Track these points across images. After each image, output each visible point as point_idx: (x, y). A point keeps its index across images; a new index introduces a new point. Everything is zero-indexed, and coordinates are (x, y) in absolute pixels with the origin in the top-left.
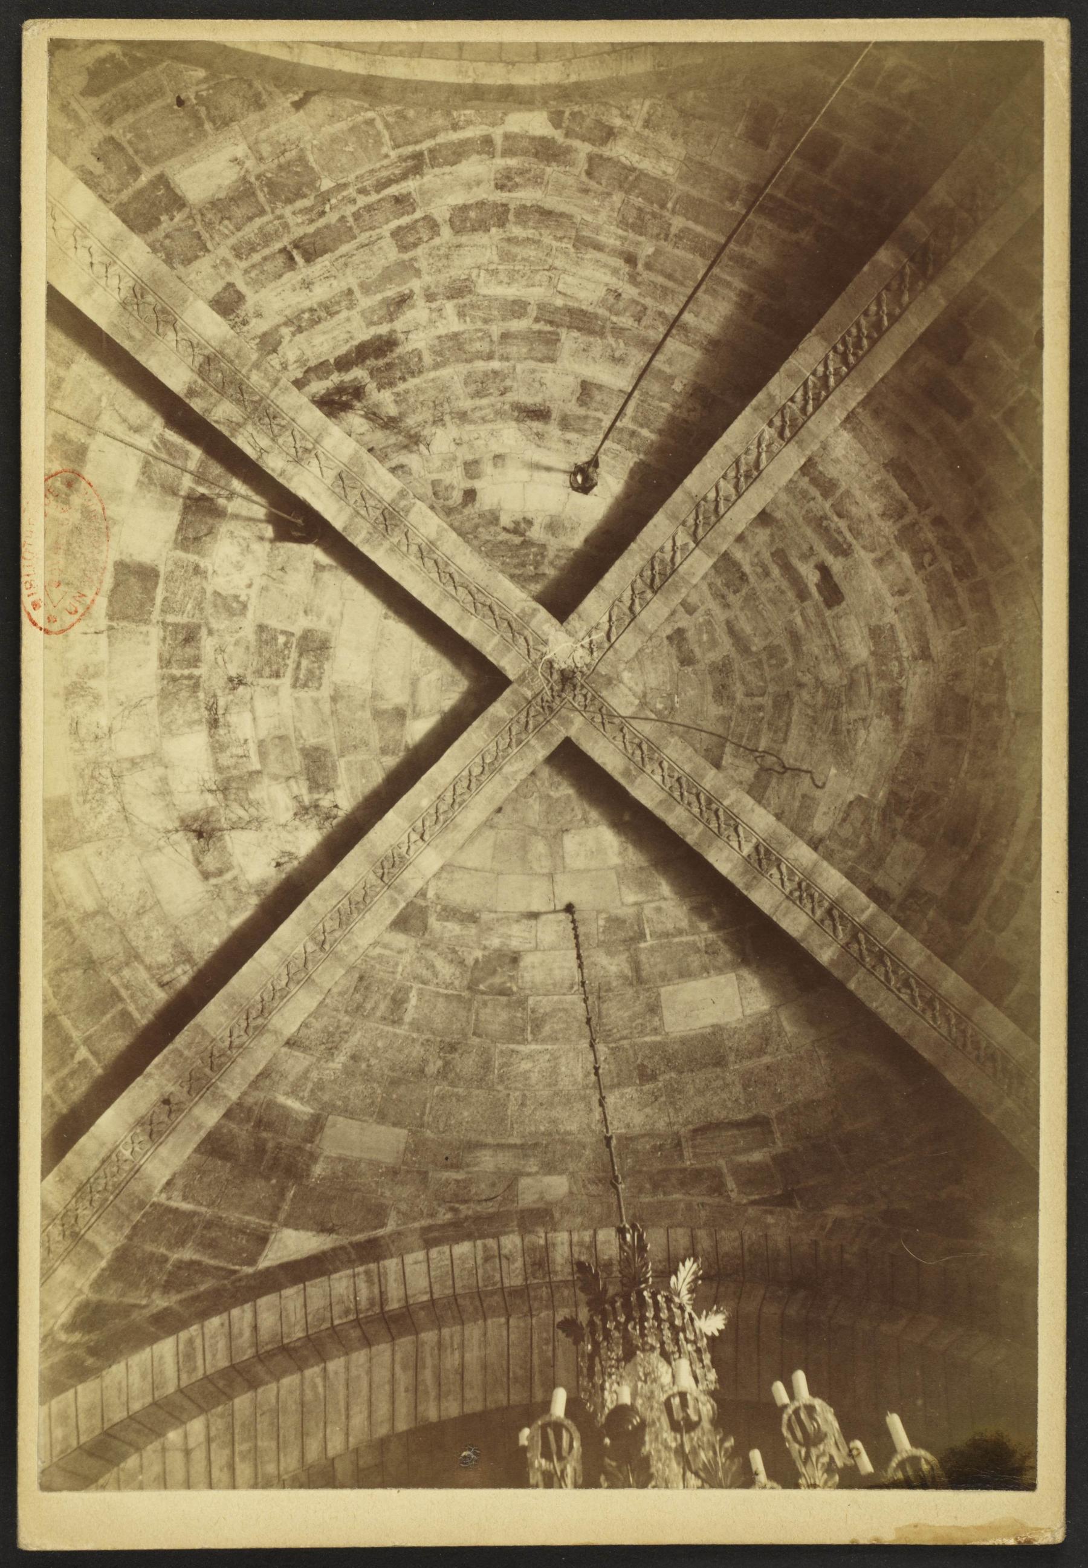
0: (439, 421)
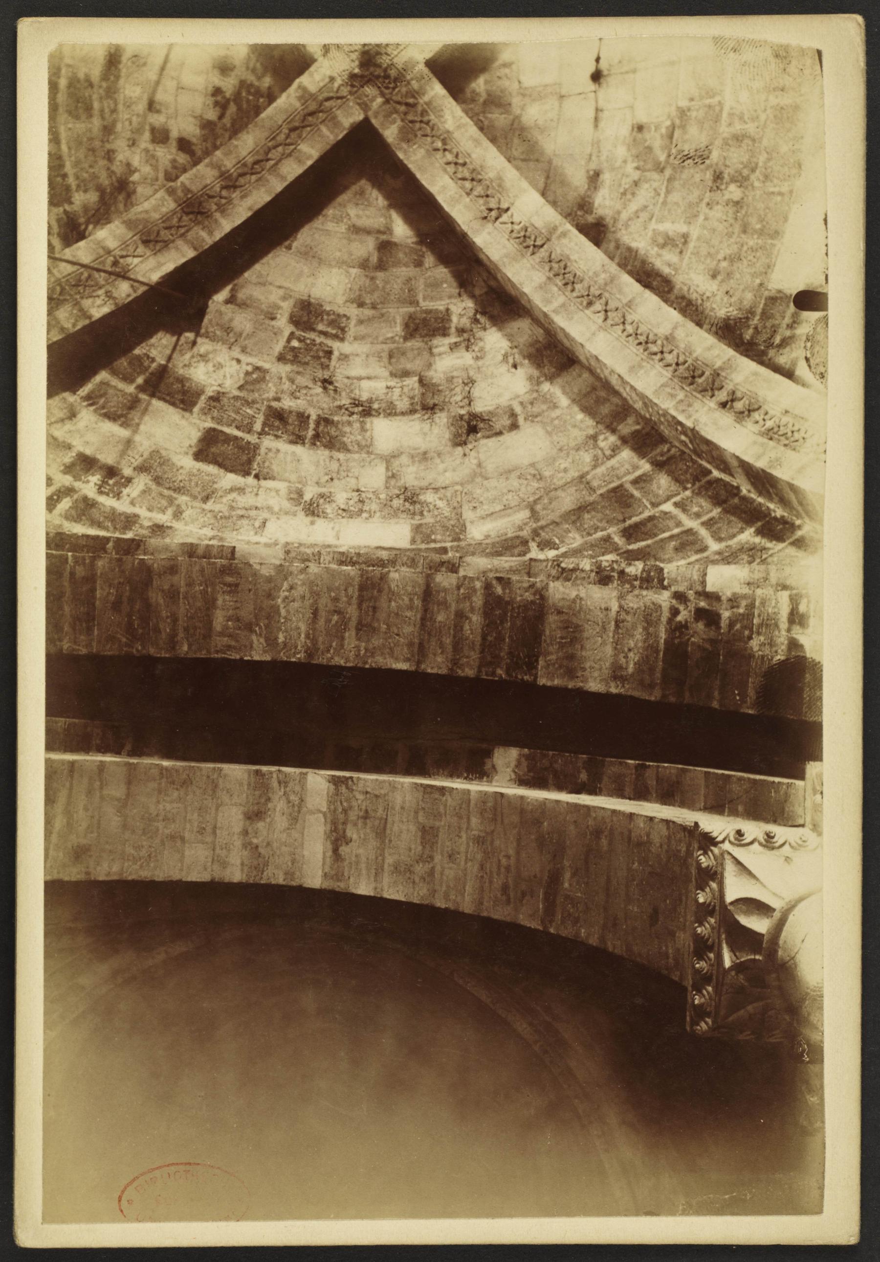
0: (109, 156)
